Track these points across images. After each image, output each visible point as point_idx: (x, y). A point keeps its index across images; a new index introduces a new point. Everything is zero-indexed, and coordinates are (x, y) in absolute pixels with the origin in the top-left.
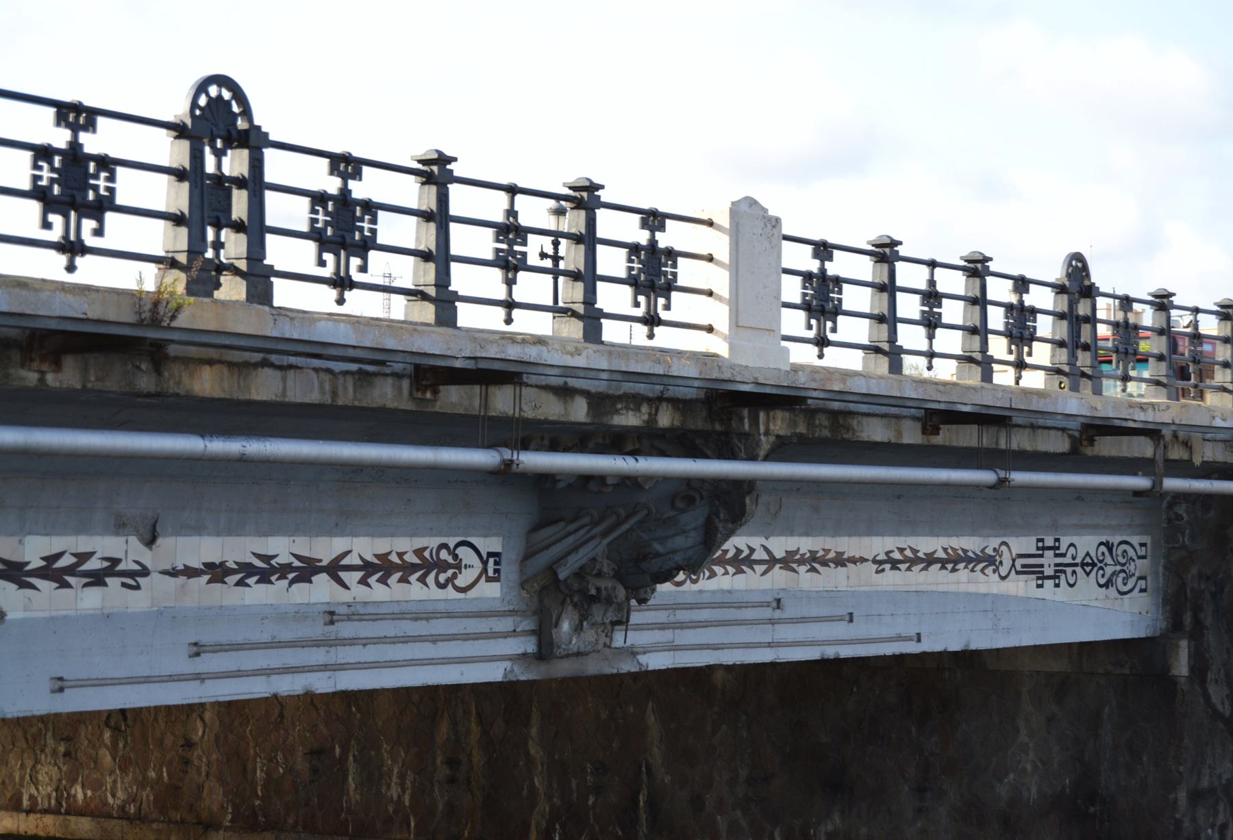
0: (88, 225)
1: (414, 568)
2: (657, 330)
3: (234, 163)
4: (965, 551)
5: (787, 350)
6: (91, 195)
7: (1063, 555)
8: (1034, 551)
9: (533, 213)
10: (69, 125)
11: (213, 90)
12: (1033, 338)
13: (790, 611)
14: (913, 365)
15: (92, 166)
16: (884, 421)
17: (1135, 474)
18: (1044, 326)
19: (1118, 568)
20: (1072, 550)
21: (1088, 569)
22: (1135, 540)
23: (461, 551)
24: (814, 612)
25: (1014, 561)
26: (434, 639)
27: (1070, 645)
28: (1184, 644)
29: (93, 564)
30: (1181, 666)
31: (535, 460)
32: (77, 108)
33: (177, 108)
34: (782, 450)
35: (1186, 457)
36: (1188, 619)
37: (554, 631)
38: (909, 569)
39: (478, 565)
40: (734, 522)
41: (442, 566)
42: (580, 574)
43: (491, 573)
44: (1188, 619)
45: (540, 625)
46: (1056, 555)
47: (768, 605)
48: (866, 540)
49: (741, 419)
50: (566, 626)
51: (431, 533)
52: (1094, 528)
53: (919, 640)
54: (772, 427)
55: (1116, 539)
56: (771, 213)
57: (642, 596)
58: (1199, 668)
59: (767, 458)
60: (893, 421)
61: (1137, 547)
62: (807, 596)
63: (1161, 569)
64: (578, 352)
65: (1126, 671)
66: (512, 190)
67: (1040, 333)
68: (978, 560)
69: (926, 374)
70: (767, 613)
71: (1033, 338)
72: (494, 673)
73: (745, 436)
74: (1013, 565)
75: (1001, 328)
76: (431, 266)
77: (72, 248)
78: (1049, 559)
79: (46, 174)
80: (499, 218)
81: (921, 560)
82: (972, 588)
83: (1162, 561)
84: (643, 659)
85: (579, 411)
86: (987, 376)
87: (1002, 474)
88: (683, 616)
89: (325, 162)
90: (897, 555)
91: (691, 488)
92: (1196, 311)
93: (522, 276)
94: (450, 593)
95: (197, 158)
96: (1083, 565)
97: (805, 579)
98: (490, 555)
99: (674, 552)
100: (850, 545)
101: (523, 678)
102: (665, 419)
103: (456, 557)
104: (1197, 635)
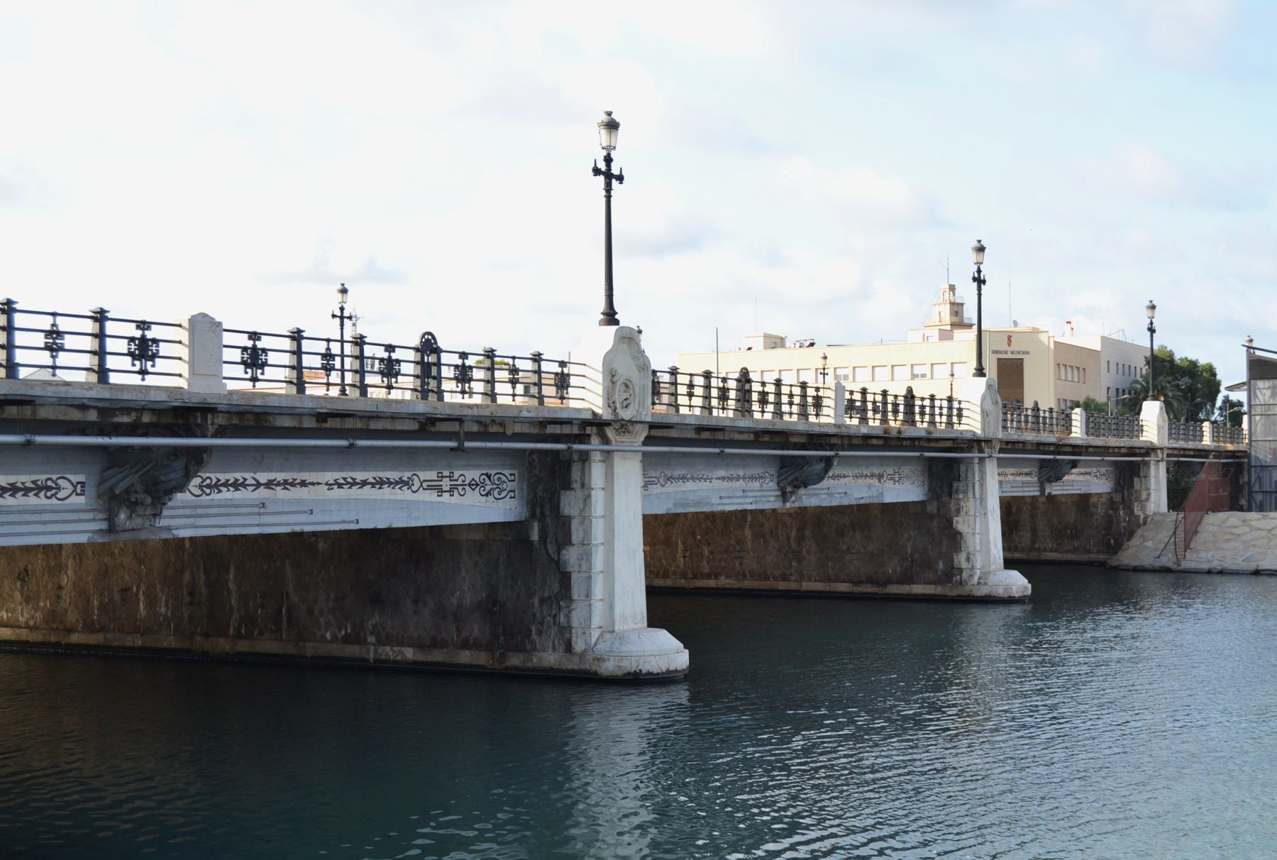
0: (149, 363)
1: (31, 490)
2: (146, 377)
4: (388, 479)
5: (225, 384)
7: (457, 480)
8: (436, 478)
9: (520, 364)
10: (141, 329)
11: (426, 337)
12: (728, 399)
13: (270, 509)
14: (683, 410)
15: (150, 343)
16: (291, 417)
17: (451, 440)
18: (732, 394)
19: (495, 486)
20: (462, 478)
21: (473, 487)
22: (507, 472)
23: (60, 482)
24: (286, 509)
25: (422, 483)
26: (45, 523)
27: (484, 524)
28: (536, 524)
29: (705, 477)
30: (535, 536)
31: (927, 454)
32: (144, 322)
33: (416, 342)
34: (221, 432)
35: (501, 430)
36: (538, 512)
37: (116, 519)
38: (350, 488)
39: (71, 488)
40: (198, 466)
41: (49, 488)
42: (127, 491)
43: (79, 491)
44: (538, 512)
45: (110, 516)
46: (451, 480)
47: (257, 506)
48: (321, 474)
49: (197, 417)
50: (122, 516)
51: (42, 473)
52: (477, 467)
53: (358, 523)
54: (216, 421)
55: (493, 472)
56: (217, 320)
57: (163, 501)
58: (543, 536)
59: (215, 436)
60: (297, 417)
61: (509, 476)
62: (283, 501)
63: (525, 487)
64: (91, 389)
65: (510, 539)
66: (54, 314)
67: (770, 401)
68: (397, 483)
69: (513, 403)
70: (256, 510)
71: (728, 399)
72: (83, 539)
73: (198, 425)
74: (421, 485)
75: (716, 396)
76: (358, 375)
77: (254, 379)
78: (446, 484)
79: (133, 347)
80: (323, 351)
81: (358, 484)
82: (393, 497)
83: (526, 483)
84: (174, 532)
85: (93, 416)
86: (711, 413)
87: (352, 441)
88: (199, 511)
90: (342, 481)
91: (176, 451)
92: (875, 394)
94: (54, 501)
95: (422, 358)
96: (470, 485)
97: (280, 492)
98: (78, 483)
99: (172, 480)
100: (309, 476)
101: (100, 541)
102: (146, 418)
103: (57, 484)
104: (542, 520)
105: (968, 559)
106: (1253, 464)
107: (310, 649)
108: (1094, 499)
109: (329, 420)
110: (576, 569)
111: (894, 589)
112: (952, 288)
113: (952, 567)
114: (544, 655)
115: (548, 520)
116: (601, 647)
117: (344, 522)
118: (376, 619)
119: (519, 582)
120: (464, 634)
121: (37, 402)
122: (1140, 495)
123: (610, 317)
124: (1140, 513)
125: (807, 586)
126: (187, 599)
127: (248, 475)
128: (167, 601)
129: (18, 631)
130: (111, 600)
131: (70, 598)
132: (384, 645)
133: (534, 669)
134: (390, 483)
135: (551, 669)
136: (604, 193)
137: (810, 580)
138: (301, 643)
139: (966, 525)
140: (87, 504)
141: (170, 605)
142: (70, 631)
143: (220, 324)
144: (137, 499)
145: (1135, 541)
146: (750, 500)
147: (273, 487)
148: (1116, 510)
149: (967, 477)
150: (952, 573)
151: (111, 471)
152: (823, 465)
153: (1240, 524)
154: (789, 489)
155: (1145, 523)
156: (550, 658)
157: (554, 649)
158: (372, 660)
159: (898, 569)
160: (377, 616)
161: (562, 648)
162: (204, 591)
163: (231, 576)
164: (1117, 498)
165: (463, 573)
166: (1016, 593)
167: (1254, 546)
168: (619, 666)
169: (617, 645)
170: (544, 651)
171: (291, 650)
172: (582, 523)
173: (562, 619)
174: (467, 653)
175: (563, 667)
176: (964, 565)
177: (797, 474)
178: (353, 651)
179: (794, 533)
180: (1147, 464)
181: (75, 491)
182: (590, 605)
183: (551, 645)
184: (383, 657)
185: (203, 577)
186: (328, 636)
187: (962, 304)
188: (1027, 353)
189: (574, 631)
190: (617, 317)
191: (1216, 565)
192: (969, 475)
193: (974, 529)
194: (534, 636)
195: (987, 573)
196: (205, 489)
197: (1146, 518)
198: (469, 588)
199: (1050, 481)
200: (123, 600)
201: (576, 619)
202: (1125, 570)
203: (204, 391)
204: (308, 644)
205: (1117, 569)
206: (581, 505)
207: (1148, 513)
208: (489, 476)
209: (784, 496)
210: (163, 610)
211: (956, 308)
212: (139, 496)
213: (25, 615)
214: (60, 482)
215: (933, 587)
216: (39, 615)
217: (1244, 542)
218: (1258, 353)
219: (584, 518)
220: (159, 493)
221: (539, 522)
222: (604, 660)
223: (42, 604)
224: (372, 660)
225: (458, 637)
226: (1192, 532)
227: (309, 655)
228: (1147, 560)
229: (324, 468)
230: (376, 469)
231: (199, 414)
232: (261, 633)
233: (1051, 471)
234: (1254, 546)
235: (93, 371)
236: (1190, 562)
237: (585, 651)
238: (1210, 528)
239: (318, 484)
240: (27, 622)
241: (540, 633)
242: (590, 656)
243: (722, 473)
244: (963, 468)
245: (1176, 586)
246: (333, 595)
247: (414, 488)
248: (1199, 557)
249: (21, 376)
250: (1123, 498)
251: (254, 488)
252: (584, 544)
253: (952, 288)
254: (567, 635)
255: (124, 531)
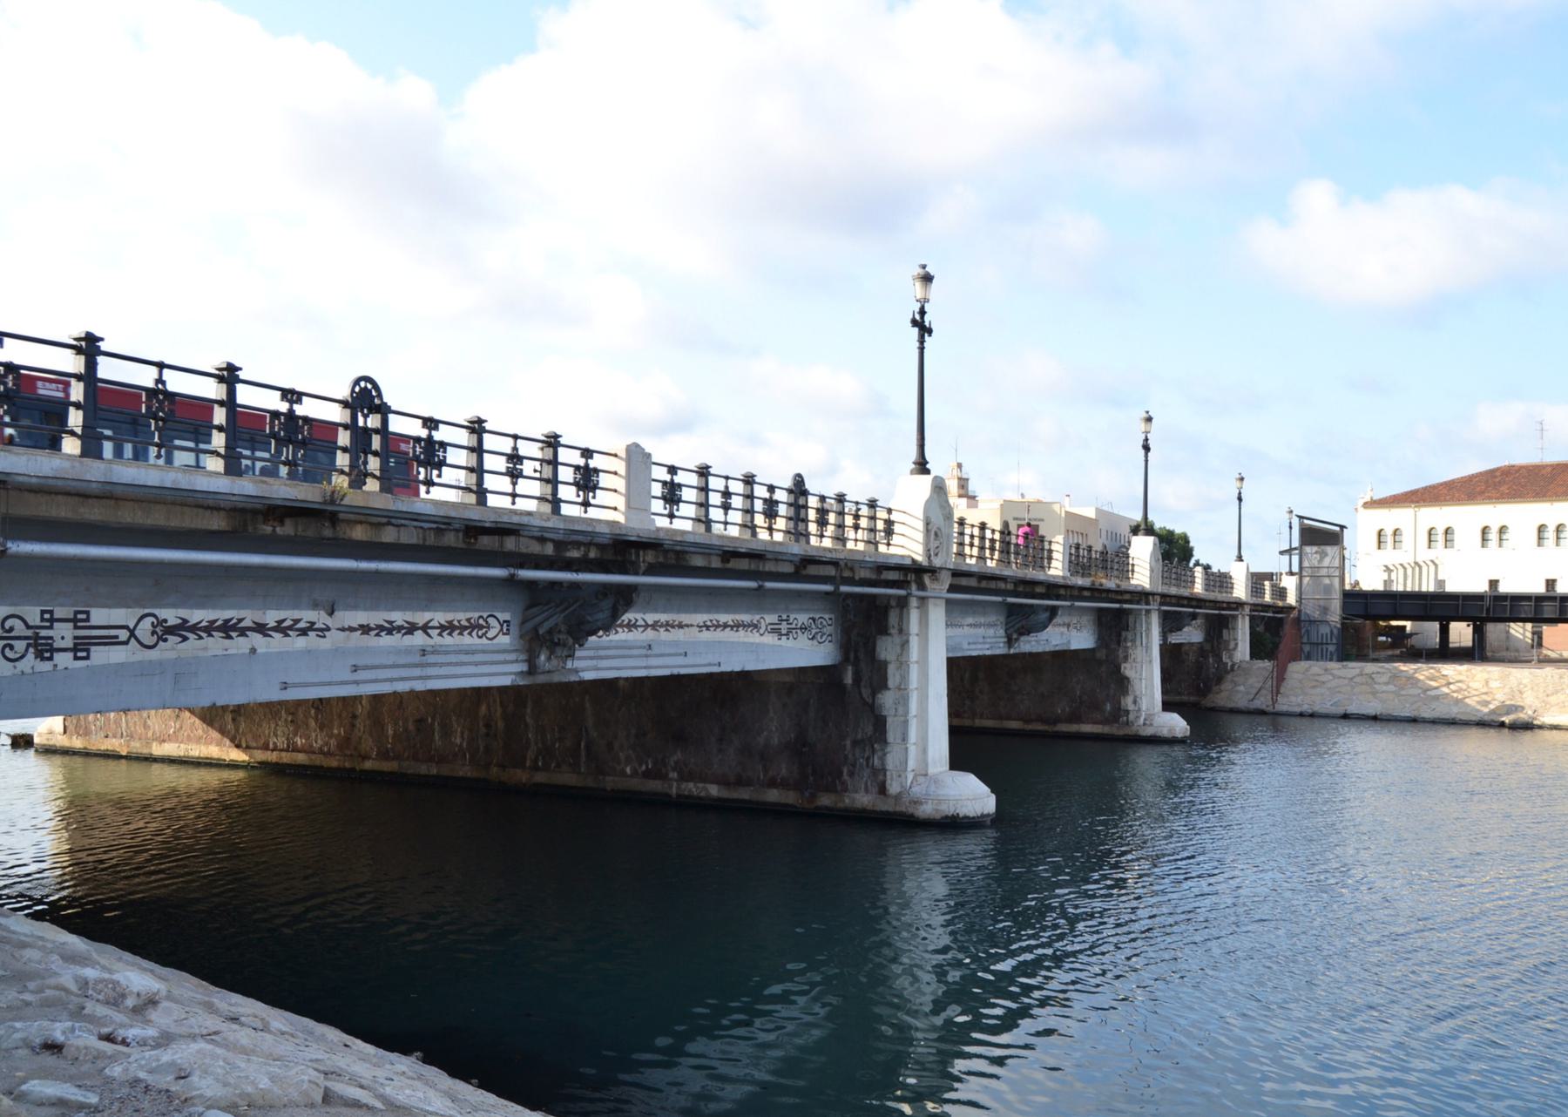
0: (435, 472)
1: (466, 628)
3: (373, 421)
5: (654, 520)
6: (436, 459)
15: (300, 422)
22: (827, 617)
26: (476, 664)
28: (850, 668)
30: (849, 679)
32: (292, 392)
34: (652, 570)
36: (852, 656)
41: (480, 627)
42: (550, 632)
43: (505, 631)
44: (852, 656)
47: (644, 647)
50: (543, 658)
52: (807, 611)
55: (817, 616)
56: (647, 451)
58: (857, 679)
62: (665, 643)
64: (548, 519)
68: (749, 626)
70: (644, 652)
72: (506, 681)
73: (633, 563)
82: (746, 640)
84: (581, 674)
85: (549, 549)
87: (760, 583)
88: (602, 653)
89: (278, 393)
90: (709, 623)
91: (606, 588)
93: (520, 481)
96: (801, 629)
97: (663, 635)
98: (505, 621)
99: (597, 620)
100: (685, 618)
101: (521, 683)
103: (487, 622)
104: (856, 664)
105: (1135, 702)
106: (1303, 618)
107: (610, 782)
108: (1185, 649)
109: (732, 560)
110: (892, 712)
111: (1064, 728)
112: (960, 466)
113: (1119, 709)
114: (857, 796)
115: (863, 665)
116: (916, 790)
117: (710, 665)
118: (678, 756)
119: (830, 724)
120: (771, 773)
121: (521, 532)
122: (1229, 645)
123: (922, 467)
124: (1228, 661)
125: (979, 723)
126: (483, 730)
127: (639, 616)
128: (462, 733)
129: (313, 757)
130: (406, 730)
131: (365, 726)
132: (687, 781)
133: (846, 810)
134: (744, 626)
135: (864, 810)
136: (917, 344)
137: (981, 717)
138: (601, 777)
139: (1134, 671)
140: (511, 644)
141: (465, 736)
142: (365, 757)
143: (649, 455)
144: (559, 639)
145: (1226, 686)
146: (987, 646)
147: (406, 625)
148: (1206, 658)
149: (1135, 627)
150: (1119, 714)
151: (535, 610)
152: (1047, 615)
153: (1323, 672)
154: (1015, 636)
155: (1232, 669)
156: (863, 799)
157: (867, 791)
158: (674, 796)
159: (1067, 709)
160: (679, 753)
161: (875, 790)
162: (501, 724)
163: (529, 710)
164: (1208, 647)
165: (771, 714)
166: (1179, 735)
167: (1339, 692)
168: (937, 810)
169: (933, 788)
170: (856, 792)
171: (590, 782)
172: (899, 668)
173: (876, 762)
174: (775, 791)
175: (877, 808)
176: (1131, 707)
177: (1024, 622)
178: (654, 785)
179: (967, 675)
180: (1235, 617)
181: (502, 630)
182: (907, 748)
183: (863, 786)
184: (686, 793)
185: (499, 710)
186: (628, 770)
187: (967, 480)
188: (1042, 520)
189: (888, 773)
190: (928, 466)
191: (1306, 708)
192: (1137, 625)
193: (1141, 675)
194: (846, 777)
195: (1151, 715)
196: (484, 624)
197: (1233, 666)
198: (777, 728)
199: (1171, 631)
200: (418, 730)
201: (891, 762)
202: (1221, 711)
203: (637, 527)
204: (609, 778)
205: (1213, 709)
206: (899, 651)
207: (1234, 660)
208: (814, 620)
209: (1010, 642)
210: (458, 741)
211: (962, 483)
212: (561, 637)
213: (319, 741)
214: (491, 620)
215: (1101, 726)
216: (333, 742)
217: (1329, 689)
218: (1306, 521)
219: (901, 663)
220: (580, 631)
221: (853, 665)
222: (921, 803)
223: (336, 731)
224: (674, 796)
225: (765, 776)
226: (1280, 677)
227: (609, 789)
228: (1241, 702)
229: (696, 610)
230: (735, 611)
231: (633, 551)
232: (558, 766)
233: (1020, 621)
234: (1339, 692)
235: (547, 500)
236: (1283, 705)
237: (900, 793)
238: (1296, 676)
239: (692, 625)
240: (321, 749)
241: (851, 774)
242: (905, 799)
243: (970, 620)
244: (1131, 619)
245: (1276, 729)
246: (633, 731)
247: (762, 631)
248: (1292, 700)
249: (489, 504)
250: (1212, 646)
251: (430, 625)
252: (900, 689)
253: (960, 466)
254: (881, 777)
255: (543, 673)
